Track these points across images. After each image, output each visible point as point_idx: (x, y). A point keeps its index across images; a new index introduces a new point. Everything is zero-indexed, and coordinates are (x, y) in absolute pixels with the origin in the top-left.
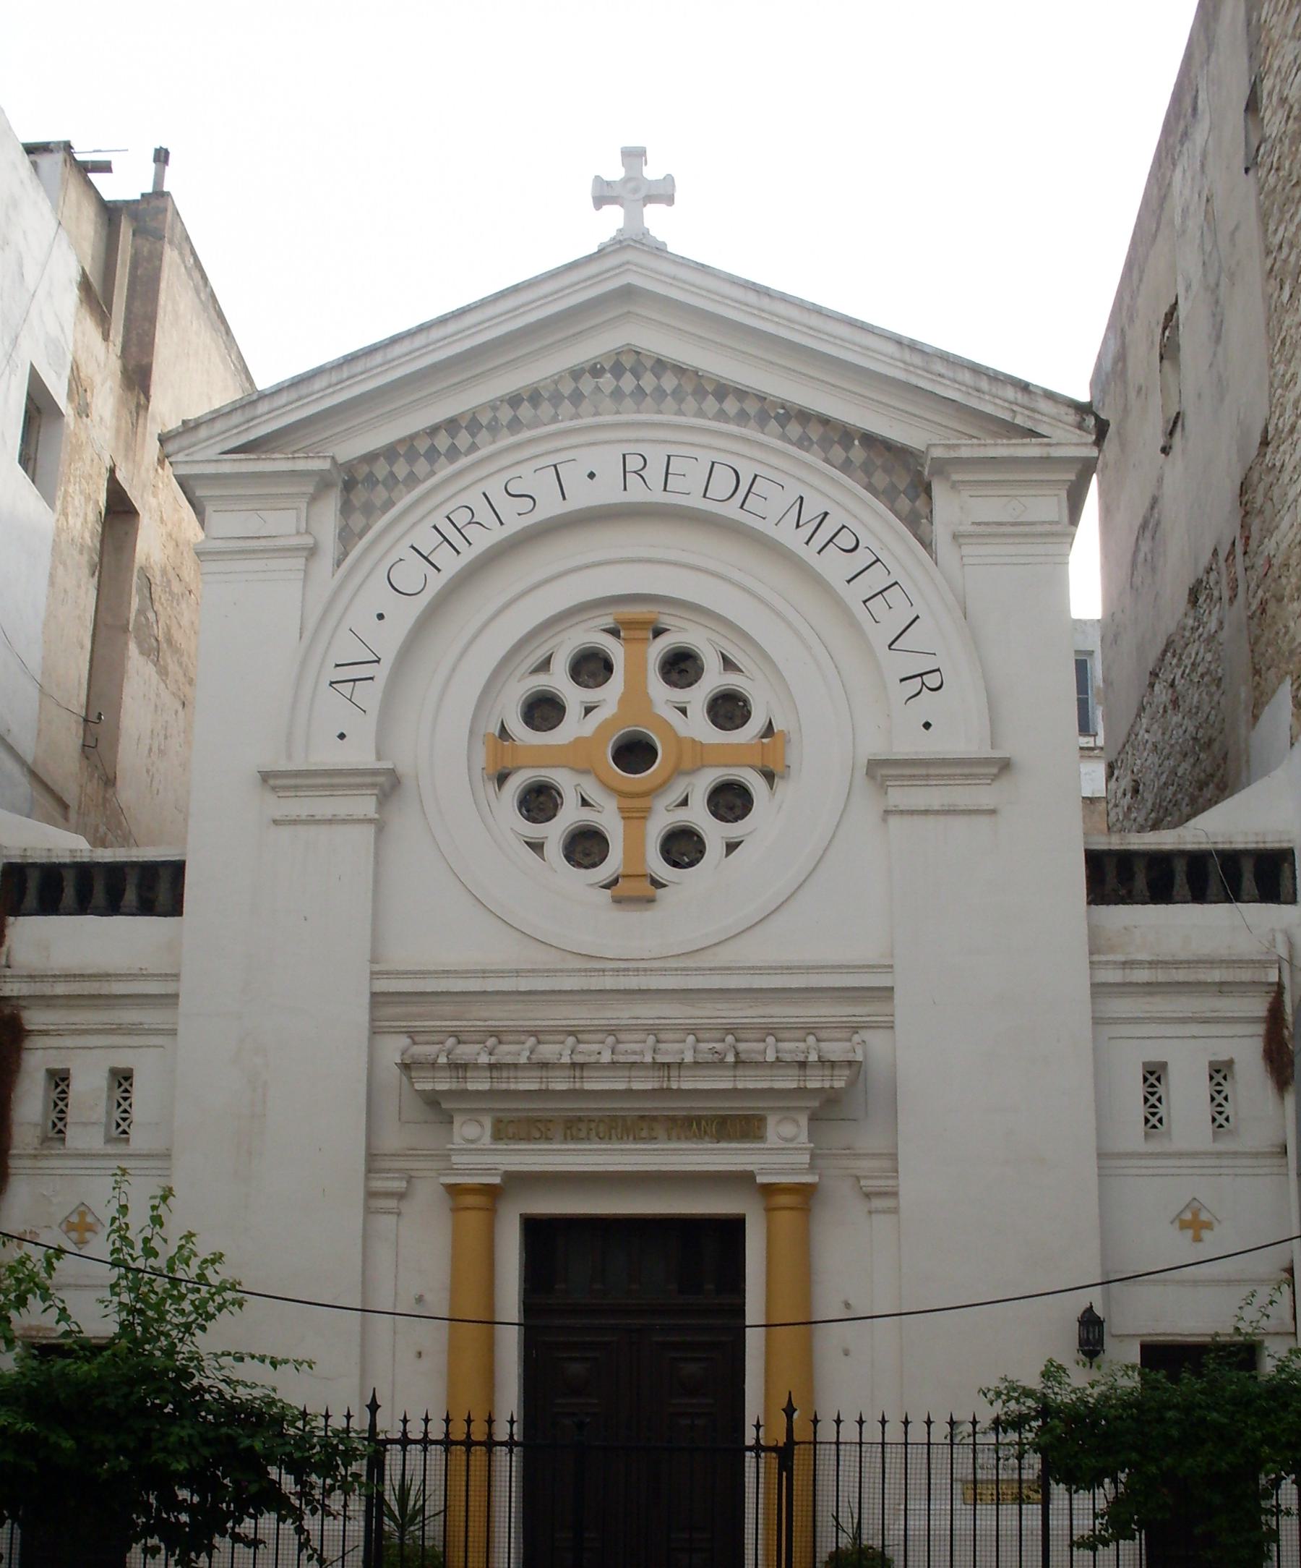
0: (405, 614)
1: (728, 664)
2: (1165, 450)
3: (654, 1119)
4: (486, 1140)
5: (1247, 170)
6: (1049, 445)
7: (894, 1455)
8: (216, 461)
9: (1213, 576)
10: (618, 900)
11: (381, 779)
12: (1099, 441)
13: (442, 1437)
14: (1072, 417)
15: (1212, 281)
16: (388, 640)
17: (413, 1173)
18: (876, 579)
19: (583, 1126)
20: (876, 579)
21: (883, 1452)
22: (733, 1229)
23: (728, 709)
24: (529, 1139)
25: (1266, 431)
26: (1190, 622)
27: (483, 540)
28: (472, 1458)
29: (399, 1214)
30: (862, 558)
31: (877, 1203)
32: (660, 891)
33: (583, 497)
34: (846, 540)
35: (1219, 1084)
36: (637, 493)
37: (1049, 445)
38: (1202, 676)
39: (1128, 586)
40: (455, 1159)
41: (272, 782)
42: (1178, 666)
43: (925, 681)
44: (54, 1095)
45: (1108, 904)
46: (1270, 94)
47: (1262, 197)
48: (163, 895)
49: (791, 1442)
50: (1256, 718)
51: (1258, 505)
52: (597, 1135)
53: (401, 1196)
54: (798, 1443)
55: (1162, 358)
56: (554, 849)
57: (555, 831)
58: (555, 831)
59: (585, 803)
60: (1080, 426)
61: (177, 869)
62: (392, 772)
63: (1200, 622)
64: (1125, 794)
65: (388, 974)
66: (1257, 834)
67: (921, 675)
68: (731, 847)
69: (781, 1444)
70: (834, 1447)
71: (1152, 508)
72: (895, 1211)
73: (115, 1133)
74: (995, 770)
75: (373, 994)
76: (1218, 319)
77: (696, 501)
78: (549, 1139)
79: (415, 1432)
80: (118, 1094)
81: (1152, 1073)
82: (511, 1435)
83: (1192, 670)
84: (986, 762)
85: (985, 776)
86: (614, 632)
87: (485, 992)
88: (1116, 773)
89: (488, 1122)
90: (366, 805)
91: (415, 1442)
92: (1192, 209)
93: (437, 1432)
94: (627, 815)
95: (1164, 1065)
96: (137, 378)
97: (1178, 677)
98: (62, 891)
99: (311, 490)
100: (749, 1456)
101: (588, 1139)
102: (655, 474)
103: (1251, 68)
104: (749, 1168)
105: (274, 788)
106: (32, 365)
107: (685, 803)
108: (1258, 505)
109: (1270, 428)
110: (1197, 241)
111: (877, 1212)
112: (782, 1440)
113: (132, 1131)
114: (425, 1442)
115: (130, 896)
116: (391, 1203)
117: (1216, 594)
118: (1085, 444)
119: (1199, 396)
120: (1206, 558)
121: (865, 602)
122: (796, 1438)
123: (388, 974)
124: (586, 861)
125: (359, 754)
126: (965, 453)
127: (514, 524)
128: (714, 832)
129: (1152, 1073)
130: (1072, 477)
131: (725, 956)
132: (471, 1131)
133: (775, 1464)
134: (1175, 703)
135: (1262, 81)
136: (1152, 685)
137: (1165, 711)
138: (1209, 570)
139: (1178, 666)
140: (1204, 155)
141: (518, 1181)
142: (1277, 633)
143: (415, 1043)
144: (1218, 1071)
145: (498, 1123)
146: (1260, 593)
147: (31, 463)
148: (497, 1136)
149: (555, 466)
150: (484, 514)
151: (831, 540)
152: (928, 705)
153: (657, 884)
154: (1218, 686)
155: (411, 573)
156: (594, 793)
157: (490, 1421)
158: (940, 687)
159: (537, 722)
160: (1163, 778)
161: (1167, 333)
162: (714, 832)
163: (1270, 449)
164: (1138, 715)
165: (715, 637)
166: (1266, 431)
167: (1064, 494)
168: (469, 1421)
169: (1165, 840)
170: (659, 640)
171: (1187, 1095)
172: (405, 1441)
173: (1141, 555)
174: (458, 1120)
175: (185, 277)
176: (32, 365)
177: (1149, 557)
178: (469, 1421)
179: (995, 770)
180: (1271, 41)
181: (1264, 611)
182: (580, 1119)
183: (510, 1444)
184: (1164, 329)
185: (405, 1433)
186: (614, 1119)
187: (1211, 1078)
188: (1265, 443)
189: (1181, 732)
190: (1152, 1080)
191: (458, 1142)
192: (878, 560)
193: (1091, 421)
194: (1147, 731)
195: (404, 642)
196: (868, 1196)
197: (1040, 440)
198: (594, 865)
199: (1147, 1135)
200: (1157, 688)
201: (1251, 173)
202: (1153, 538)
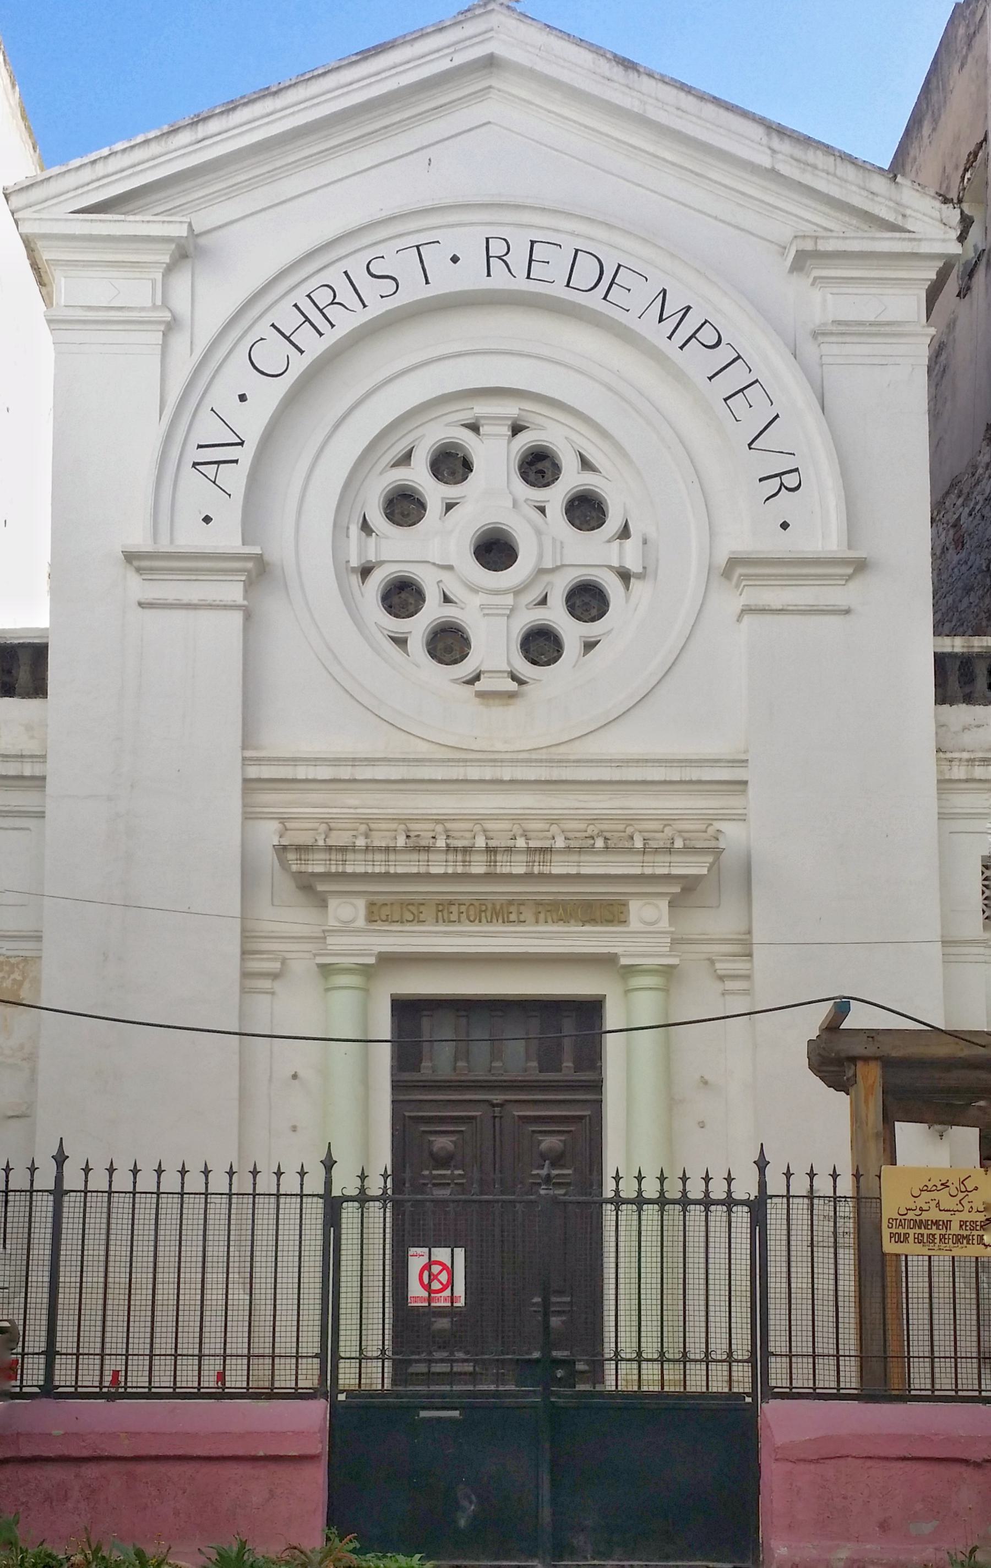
0: (268, 396)
3: (522, 903)
4: (361, 922)
6: (910, 240)
7: (146, 1206)
8: (66, 220)
10: (481, 695)
11: (250, 565)
16: (252, 423)
17: (288, 955)
18: (736, 377)
19: (454, 909)
20: (736, 377)
22: (590, 1010)
23: (586, 510)
27: (346, 322)
30: (723, 355)
31: (730, 985)
32: (525, 687)
33: (447, 280)
34: (708, 336)
36: (500, 280)
41: (136, 563)
43: (784, 482)
48: (23, 675)
53: (275, 976)
54: (771, 1197)
56: (417, 644)
57: (418, 627)
58: (418, 627)
59: (447, 599)
62: (260, 560)
65: (259, 761)
68: (589, 646)
75: (246, 781)
77: (558, 290)
84: (844, 562)
85: (841, 576)
86: (474, 427)
87: (355, 781)
89: (361, 904)
90: (233, 592)
91: (674, 1202)
93: (651, 1190)
94: (486, 611)
97: (965, 514)
99: (167, 259)
100: (609, 1209)
102: (518, 259)
104: (613, 950)
105: (138, 570)
107: (544, 601)
111: (733, 993)
114: (707, 1202)
121: (725, 400)
123: (259, 761)
124: (447, 657)
125: (226, 537)
127: (377, 308)
128: (571, 631)
131: (592, 748)
141: (389, 961)
145: (371, 905)
148: (370, 919)
149: (418, 247)
150: (344, 293)
155: (273, 353)
156: (455, 590)
158: (800, 484)
159: (398, 517)
161: (968, 175)
162: (571, 631)
165: (574, 437)
170: (520, 436)
174: (333, 903)
179: (850, 571)
182: (451, 903)
184: (966, 170)
185: (362, 1190)
186: (482, 903)
189: (964, 568)
192: (739, 357)
195: (269, 424)
196: (721, 978)
198: (455, 662)
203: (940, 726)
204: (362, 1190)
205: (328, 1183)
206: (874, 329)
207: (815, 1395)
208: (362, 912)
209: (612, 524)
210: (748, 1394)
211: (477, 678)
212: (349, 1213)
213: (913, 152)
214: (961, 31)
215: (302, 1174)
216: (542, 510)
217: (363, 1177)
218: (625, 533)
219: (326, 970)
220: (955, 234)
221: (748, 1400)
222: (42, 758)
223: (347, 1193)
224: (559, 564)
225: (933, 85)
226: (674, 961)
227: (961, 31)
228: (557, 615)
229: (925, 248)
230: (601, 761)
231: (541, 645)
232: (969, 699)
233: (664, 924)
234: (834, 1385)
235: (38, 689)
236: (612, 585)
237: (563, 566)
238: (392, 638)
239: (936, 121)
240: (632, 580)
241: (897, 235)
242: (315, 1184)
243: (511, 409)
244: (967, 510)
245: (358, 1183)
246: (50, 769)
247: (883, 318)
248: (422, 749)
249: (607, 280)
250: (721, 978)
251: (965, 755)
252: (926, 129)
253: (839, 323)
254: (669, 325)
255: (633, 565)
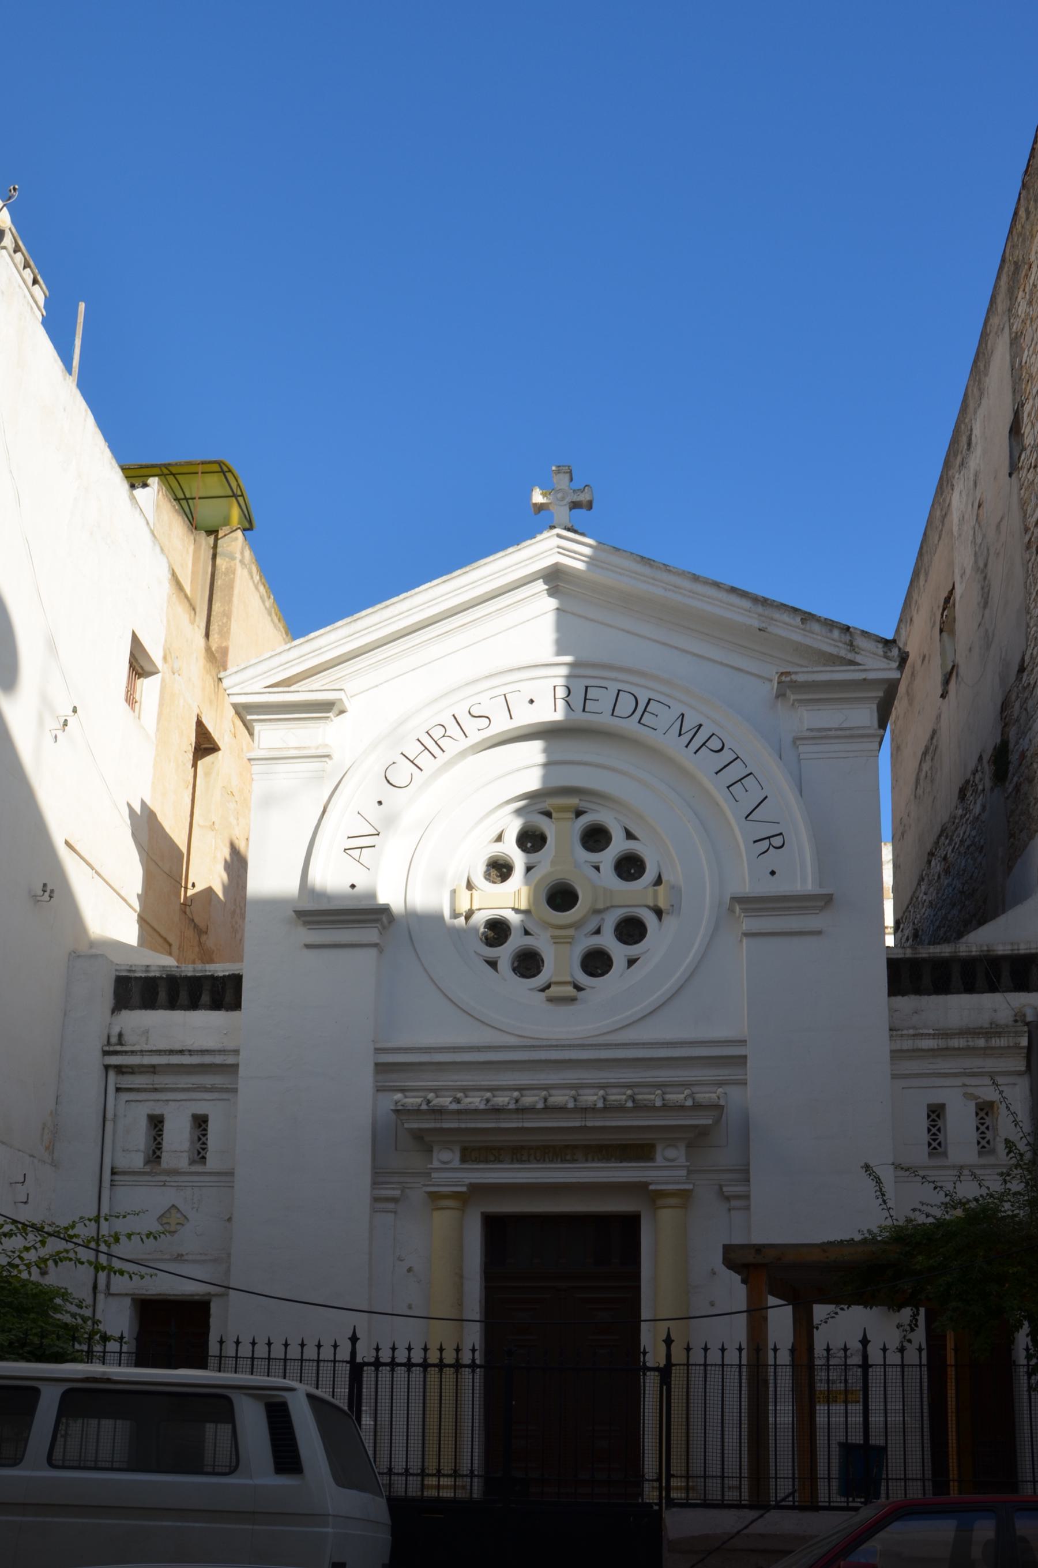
1: (630, 836)
2: (943, 696)
3: (576, 1147)
4: (456, 1163)
5: (1010, 475)
6: (865, 670)
9: (978, 776)
10: (551, 1000)
12: (901, 666)
13: (437, 1361)
14: (880, 649)
15: (981, 565)
18: (736, 771)
20: (736, 771)
21: (723, 1469)
23: (630, 867)
24: (487, 1161)
25: (1023, 660)
26: (960, 812)
28: (428, 1376)
29: (395, 1212)
30: (727, 756)
31: (734, 1203)
32: (582, 993)
35: (982, 1118)
37: (865, 670)
38: (968, 847)
39: (912, 797)
40: (434, 1175)
42: (949, 844)
44: (154, 1133)
45: (903, 995)
46: (1029, 414)
47: (1022, 491)
48: (229, 997)
49: (669, 1364)
50: (1010, 868)
51: (1016, 714)
52: (535, 1158)
53: (395, 1200)
55: (941, 631)
56: (505, 965)
60: (886, 657)
61: (236, 981)
63: (967, 810)
64: (907, 940)
66: (1012, 944)
67: (769, 838)
68: (631, 962)
69: (662, 1365)
70: (702, 1368)
71: (932, 738)
72: (748, 1208)
73: (196, 1158)
74: (823, 904)
76: (986, 590)
78: (500, 1161)
79: (385, 1356)
80: (198, 1133)
81: (933, 1112)
82: (473, 1360)
83: (960, 846)
86: (548, 814)
88: (902, 926)
91: (385, 1364)
92: (966, 517)
95: (942, 1106)
96: (217, 659)
97: (950, 851)
98: (157, 993)
101: (529, 1161)
103: (1014, 400)
106: (134, 633)
107: (598, 932)
108: (1016, 714)
109: (1027, 658)
110: (971, 538)
111: (734, 1209)
112: (662, 1363)
113: (208, 1156)
114: (409, 1365)
115: (205, 998)
116: (391, 1206)
117: (980, 787)
118: (890, 669)
119: (970, 650)
120: (972, 764)
122: (674, 1361)
126: (801, 678)
128: (619, 952)
129: (933, 1112)
130: (881, 694)
132: (446, 1156)
133: (657, 1380)
134: (947, 871)
135: (1023, 406)
136: (929, 862)
137: (939, 877)
138: (975, 772)
139: (949, 844)
140: (976, 475)
141: (477, 1190)
142: (1029, 805)
143: (406, 1097)
144: (982, 1110)
146: (1015, 779)
147: (137, 705)
148: (464, 1160)
151: (704, 744)
152: (773, 858)
153: (578, 988)
154: (980, 852)
157: (458, 1350)
160: (937, 923)
162: (619, 952)
163: (1025, 674)
164: (919, 884)
166: (1023, 660)
167: (875, 707)
168: (409, 1349)
169: (944, 950)
171: (961, 1123)
172: (377, 1364)
173: (923, 774)
174: (436, 1149)
175: (252, 588)
176: (134, 633)
177: (929, 774)
178: (409, 1349)
180: (1031, 376)
181: (1018, 791)
182: (522, 1148)
183: (473, 1366)
184: (944, 610)
185: (377, 1358)
187: (977, 1114)
188: (1022, 669)
189: (950, 889)
190: (934, 1116)
191: (436, 1164)
193: (895, 652)
194: (925, 894)
196: (728, 1199)
197: (857, 667)
198: (534, 976)
199: (930, 1155)
200: (933, 863)
201: (1014, 476)
202: (932, 759)
203: (892, 1011)
204: (377, 1358)
205: (353, 1353)
206: (839, 733)
207: (706, 1505)
208: (457, 1156)
209: (649, 876)
210: (656, 1504)
211: (548, 987)
212: (368, 1373)
213: (915, 596)
214: (938, 513)
215: (335, 1346)
216: (597, 868)
217: (377, 1349)
218: (659, 881)
219: (434, 1196)
220: (895, 665)
221: (656, 1508)
222: (236, 1052)
223: (366, 1360)
224: (608, 905)
225: (924, 550)
226: (690, 1187)
227: (938, 513)
228: (608, 941)
229: (871, 676)
230: (637, 1044)
231: (597, 963)
232: (918, 991)
233: (682, 1161)
234: (719, 1498)
235: (236, 1005)
236: (649, 919)
237: (612, 906)
238: (487, 962)
239: (927, 574)
240: (664, 915)
241: (852, 668)
242: (344, 1353)
243: (574, 801)
244: (951, 848)
245: (374, 1353)
246: (242, 1059)
247: (844, 725)
248: (513, 1041)
249: (642, 710)
250: (728, 1199)
251: (911, 1032)
252: (922, 582)
253: (811, 730)
254: (686, 738)
255: (662, 904)
